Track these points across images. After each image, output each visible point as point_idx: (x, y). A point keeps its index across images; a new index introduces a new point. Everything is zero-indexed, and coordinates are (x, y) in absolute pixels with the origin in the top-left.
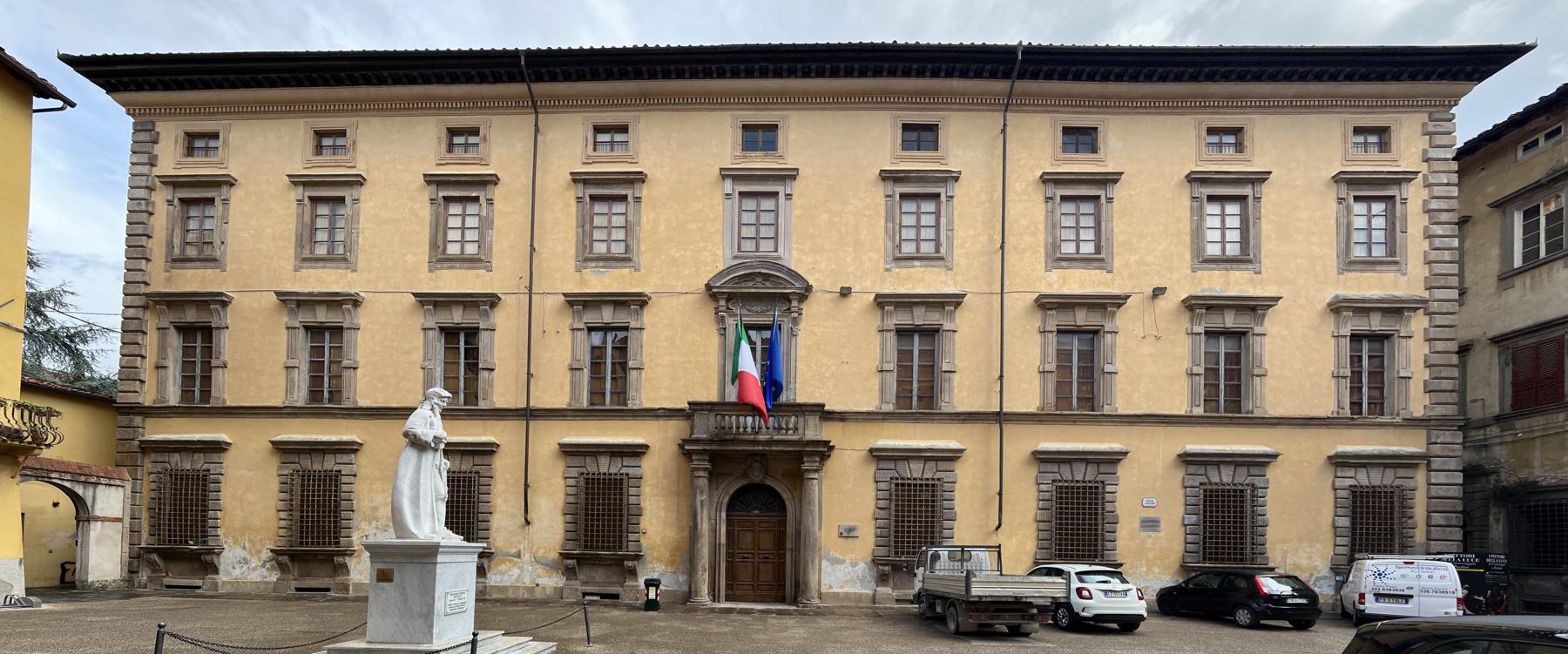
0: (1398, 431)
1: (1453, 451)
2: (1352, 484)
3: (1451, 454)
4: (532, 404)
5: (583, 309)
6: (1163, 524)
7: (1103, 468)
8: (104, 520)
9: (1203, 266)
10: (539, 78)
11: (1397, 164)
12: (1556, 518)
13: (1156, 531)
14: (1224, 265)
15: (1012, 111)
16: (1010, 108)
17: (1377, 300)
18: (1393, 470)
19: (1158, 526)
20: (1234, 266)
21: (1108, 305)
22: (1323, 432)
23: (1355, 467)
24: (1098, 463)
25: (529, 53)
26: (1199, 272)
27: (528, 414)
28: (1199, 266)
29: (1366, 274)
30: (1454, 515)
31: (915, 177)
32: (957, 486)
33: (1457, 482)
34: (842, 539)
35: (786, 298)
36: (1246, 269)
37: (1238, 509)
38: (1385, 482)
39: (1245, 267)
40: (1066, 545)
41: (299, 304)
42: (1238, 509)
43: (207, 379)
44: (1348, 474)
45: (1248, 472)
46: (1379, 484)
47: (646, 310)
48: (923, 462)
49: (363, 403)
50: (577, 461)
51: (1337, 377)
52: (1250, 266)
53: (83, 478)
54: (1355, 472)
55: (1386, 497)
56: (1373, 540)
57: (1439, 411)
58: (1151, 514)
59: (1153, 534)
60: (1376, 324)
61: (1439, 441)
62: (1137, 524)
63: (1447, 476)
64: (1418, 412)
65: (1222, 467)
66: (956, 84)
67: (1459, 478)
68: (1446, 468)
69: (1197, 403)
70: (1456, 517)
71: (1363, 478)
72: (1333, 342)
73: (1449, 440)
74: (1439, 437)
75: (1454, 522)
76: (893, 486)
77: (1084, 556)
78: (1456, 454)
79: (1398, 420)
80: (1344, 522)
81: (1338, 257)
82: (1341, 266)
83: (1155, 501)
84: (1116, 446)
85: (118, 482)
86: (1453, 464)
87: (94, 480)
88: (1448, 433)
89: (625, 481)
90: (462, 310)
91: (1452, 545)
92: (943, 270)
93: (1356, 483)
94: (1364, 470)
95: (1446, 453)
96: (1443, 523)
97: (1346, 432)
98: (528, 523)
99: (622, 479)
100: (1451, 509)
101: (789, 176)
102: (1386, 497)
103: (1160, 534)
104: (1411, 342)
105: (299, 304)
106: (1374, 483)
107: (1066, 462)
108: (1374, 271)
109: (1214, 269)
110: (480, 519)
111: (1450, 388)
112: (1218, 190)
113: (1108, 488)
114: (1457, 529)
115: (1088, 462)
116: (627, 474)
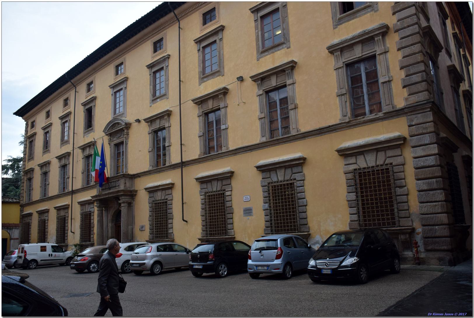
0: (386, 122)
1: (426, 128)
2: (355, 168)
3: (425, 131)
4: (73, 189)
5: (341, 54)
6: (254, 211)
7: (295, 170)
8: (14, 239)
9: (263, 54)
10: (72, 79)
11: (219, 22)
12: (278, 201)
13: (250, 215)
14: (272, 51)
15: (181, 20)
16: (179, 20)
17: (350, 39)
18: (383, 153)
19: (252, 212)
20: (276, 49)
21: (334, 52)
22: (334, 135)
23: (206, 183)
24: (291, 167)
25: (170, 2)
26: (261, 59)
27: (182, 165)
28: (260, 56)
29: (351, 22)
30: (434, 180)
31: (156, 63)
32: (173, 201)
33: (433, 152)
34: (141, 231)
35: (122, 130)
36: (283, 48)
37: (287, 197)
38: (378, 163)
39: (281, 47)
40: (383, 215)
41: (342, 50)
42: (287, 197)
43: (286, 118)
44: (351, 162)
45: (292, 171)
46: (374, 164)
47: (227, 96)
48: (375, 153)
49: (303, 130)
50: (204, 186)
51: (340, 95)
52: (284, 46)
53: (9, 228)
54: (207, 185)
55: (373, 174)
56: (368, 208)
57: (414, 99)
58: (248, 206)
59: (250, 217)
60: (358, 52)
61: (413, 123)
62: (242, 212)
63: (423, 150)
64: (400, 103)
65: (278, 171)
66: (162, 20)
67: (434, 149)
68: (422, 143)
69: (225, 146)
70: (437, 181)
71: (362, 163)
72: (335, 73)
73: (421, 121)
74: (413, 121)
75: (435, 186)
76: (154, 205)
77: (282, 231)
78: (429, 131)
79: (380, 114)
80: (353, 196)
81: (333, 19)
82: (335, 23)
83: (249, 197)
84: (227, 169)
85: (18, 228)
86: (427, 139)
87: (12, 228)
88: (420, 115)
89: (390, 169)
90: (361, 45)
91: (436, 205)
92: (166, 99)
93: (357, 167)
94: (362, 156)
95: (421, 132)
96: (425, 188)
97: (349, 132)
98: (74, 233)
99: (388, 169)
100: (431, 176)
101: (222, 28)
102: (373, 174)
103: (253, 217)
104: (389, 55)
105: (342, 50)
106: (370, 165)
107: (204, 183)
108: (356, 17)
109: (267, 55)
110: (300, 211)
111: (420, 79)
112: (264, 11)
113: (228, 193)
114: (438, 191)
115: (286, 167)
116: (391, 164)
